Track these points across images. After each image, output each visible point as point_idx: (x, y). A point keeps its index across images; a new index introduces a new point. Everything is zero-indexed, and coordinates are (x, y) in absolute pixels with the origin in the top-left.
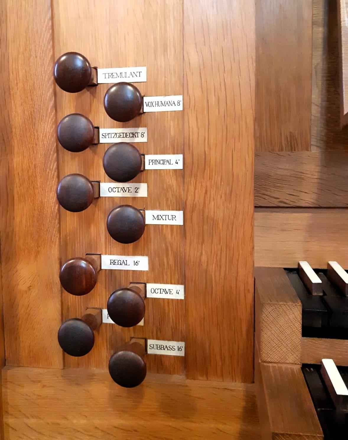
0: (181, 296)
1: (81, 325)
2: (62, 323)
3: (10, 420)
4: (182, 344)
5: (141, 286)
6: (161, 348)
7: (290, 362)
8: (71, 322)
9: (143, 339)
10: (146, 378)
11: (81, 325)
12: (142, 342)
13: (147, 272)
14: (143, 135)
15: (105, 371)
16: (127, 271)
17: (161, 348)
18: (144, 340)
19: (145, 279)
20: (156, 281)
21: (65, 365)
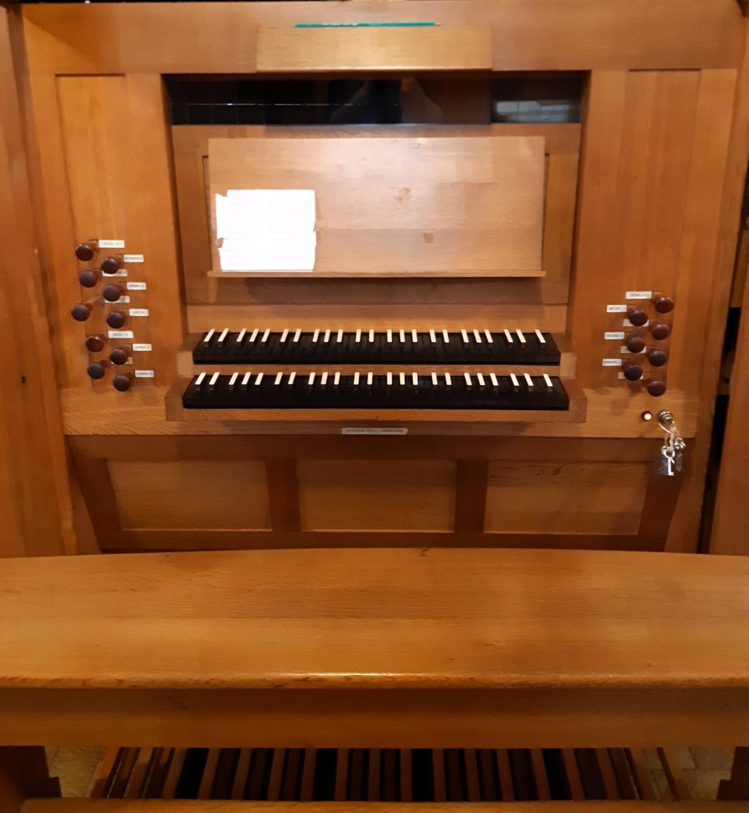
0: (150, 349)
1: (99, 366)
2: (90, 363)
3: (66, 414)
4: (152, 371)
5: (129, 346)
6: (142, 374)
7: (499, 336)
8: (94, 364)
9: (57, 86)
10: (662, 396)
11: (99, 366)
12: (132, 372)
13: (132, 339)
14: (125, 273)
15: (112, 387)
16: (122, 339)
17: (142, 374)
18: (63, 80)
19: (131, 342)
20: (138, 342)
21: (93, 385)
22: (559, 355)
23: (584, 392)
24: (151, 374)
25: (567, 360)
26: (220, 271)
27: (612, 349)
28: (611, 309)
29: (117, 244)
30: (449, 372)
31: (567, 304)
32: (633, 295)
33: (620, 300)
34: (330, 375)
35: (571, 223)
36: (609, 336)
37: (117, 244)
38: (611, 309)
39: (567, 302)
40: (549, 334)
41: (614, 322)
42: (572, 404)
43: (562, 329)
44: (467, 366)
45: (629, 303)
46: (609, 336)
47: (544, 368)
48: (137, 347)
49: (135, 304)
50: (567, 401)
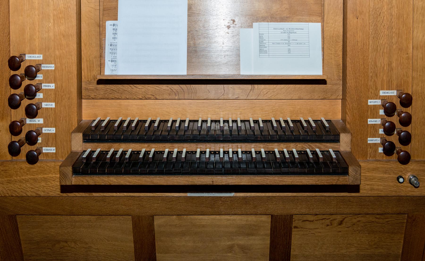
6: (48, 150)
22: (339, 135)
23: (75, 129)
24: (54, 150)
25: (344, 138)
26: (104, 75)
27: (374, 113)
28: (371, 102)
29: (38, 57)
30: (264, 148)
31: (342, 99)
32: (384, 93)
33: (376, 96)
34: (179, 150)
35: (341, 44)
36: (371, 121)
37: (38, 57)
38: (371, 102)
39: (341, 98)
40: (330, 120)
41: (374, 110)
42: (351, 170)
43: (339, 117)
44: (276, 144)
45: (383, 99)
46: (371, 121)
47: (328, 145)
48: (45, 130)
49: (45, 100)
50: (347, 168)
